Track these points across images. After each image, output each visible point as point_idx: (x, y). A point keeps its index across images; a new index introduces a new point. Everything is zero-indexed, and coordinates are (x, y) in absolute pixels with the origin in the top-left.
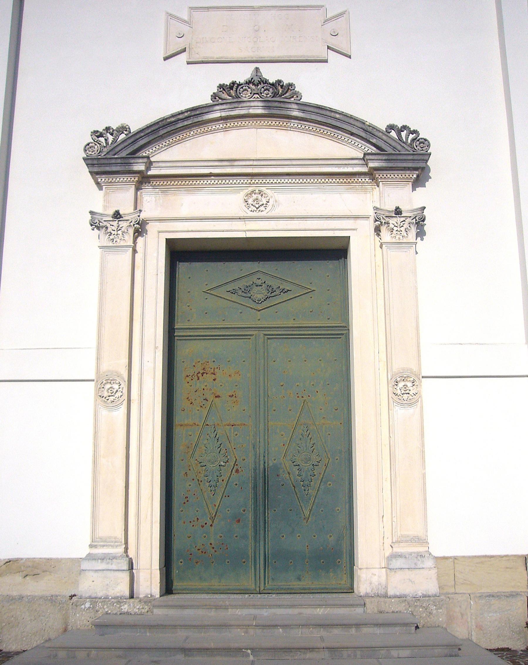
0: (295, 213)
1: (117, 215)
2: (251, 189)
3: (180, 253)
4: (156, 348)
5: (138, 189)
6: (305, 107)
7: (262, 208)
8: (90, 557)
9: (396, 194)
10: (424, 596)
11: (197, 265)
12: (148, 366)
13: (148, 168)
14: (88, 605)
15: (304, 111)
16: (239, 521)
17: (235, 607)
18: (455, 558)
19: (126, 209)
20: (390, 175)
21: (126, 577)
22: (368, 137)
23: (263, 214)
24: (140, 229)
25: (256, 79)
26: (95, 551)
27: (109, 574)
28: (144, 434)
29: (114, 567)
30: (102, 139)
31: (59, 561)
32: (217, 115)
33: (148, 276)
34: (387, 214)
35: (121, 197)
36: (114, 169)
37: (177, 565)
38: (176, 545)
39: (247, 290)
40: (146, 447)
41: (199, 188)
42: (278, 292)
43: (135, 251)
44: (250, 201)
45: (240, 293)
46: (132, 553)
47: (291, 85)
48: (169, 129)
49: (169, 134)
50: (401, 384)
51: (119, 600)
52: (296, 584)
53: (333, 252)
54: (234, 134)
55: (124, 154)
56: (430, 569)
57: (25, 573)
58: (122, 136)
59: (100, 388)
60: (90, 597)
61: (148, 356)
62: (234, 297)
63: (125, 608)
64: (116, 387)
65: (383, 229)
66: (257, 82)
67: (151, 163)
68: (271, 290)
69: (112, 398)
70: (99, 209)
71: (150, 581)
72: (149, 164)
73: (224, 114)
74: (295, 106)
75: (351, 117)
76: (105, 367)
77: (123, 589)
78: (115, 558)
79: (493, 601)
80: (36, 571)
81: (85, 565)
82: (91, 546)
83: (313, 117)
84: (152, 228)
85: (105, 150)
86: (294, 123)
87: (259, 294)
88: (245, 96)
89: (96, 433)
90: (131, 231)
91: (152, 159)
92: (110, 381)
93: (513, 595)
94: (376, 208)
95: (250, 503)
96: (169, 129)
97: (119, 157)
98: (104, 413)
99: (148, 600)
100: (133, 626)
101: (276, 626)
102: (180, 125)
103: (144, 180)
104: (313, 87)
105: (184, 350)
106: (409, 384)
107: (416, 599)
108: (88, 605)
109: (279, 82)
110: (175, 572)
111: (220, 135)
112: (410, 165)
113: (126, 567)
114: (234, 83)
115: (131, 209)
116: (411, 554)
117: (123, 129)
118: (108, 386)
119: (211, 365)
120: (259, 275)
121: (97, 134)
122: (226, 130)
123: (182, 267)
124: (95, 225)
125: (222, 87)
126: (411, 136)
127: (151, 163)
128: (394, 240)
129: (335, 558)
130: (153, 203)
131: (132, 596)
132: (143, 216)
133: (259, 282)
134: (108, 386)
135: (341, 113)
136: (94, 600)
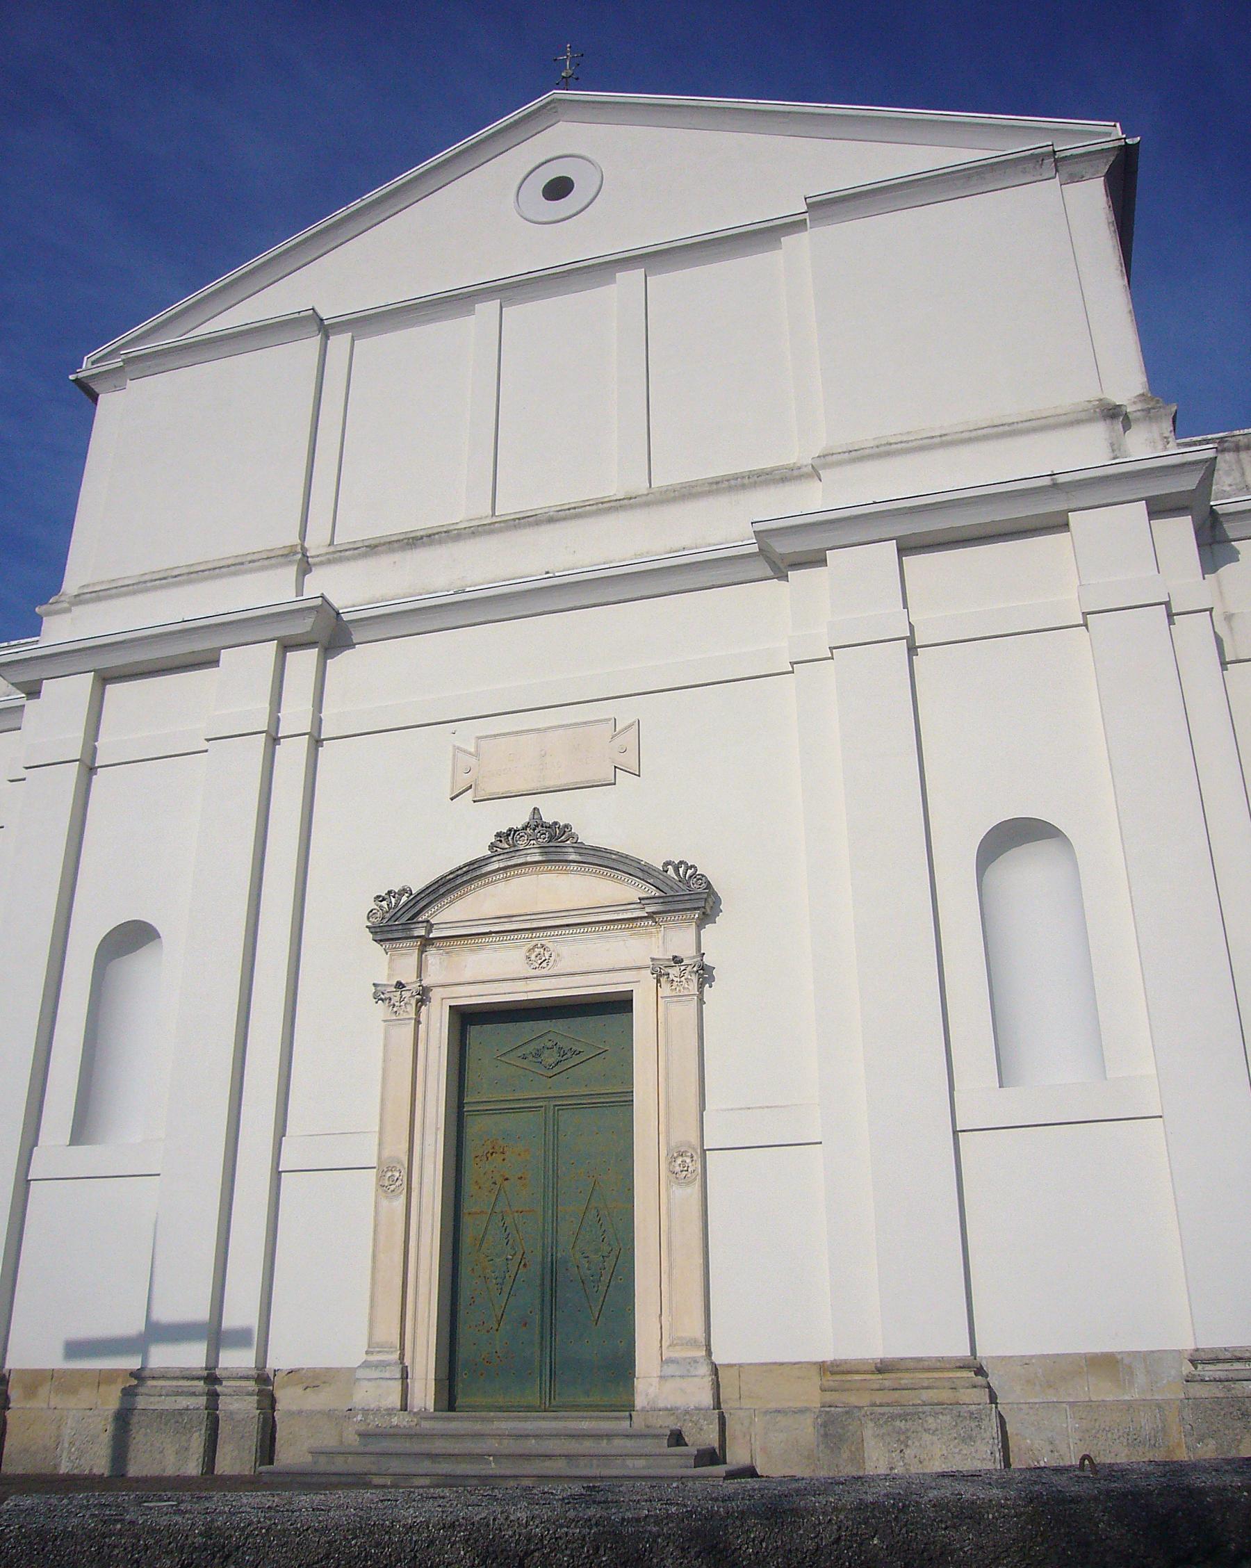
0: (580, 967)
1: (400, 985)
2: (533, 943)
3: (466, 1019)
4: (437, 1129)
5: (422, 951)
6: (581, 848)
7: (544, 964)
8: (366, 1365)
9: (677, 938)
10: (697, 1409)
11: (488, 1027)
12: (429, 1150)
13: (430, 931)
14: (359, 1417)
15: (580, 854)
16: (525, 1325)
17: (499, 1419)
18: (740, 1365)
19: (409, 977)
20: (669, 916)
21: (397, 1385)
22: (645, 877)
23: (544, 972)
24: (423, 997)
25: (533, 824)
26: (374, 1358)
27: (383, 1383)
28: (423, 1226)
29: (387, 1375)
30: (385, 904)
31: (338, 1370)
32: (496, 866)
33: (430, 1048)
34: (667, 963)
35: (405, 964)
36: (396, 935)
37: (462, 1375)
38: (463, 1353)
39: (538, 1054)
40: (426, 1240)
41: (481, 948)
42: (569, 1054)
43: (418, 1022)
44: (533, 957)
45: (531, 1058)
46: (407, 1362)
47: (566, 826)
48: (449, 886)
49: (449, 891)
50: (679, 1161)
51: (390, 1412)
52: (583, 1400)
53: (618, 1006)
54: (515, 882)
55: (403, 920)
56: (703, 1377)
57: (305, 1385)
58: (404, 899)
59: (380, 1178)
60: (363, 1409)
61: (430, 1139)
62: (525, 1064)
63: (395, 1421)
64: (397, 1174)
65: (663, 980)
66: (536, 825)
67: (432, 925)
68: (562, 1053)
69: (392, 1187)
70: (382, 980)
71: (424, 1393)
72: (430, 926)
73: (502, 865)
74: (571, 850)
75: (627, 857)
76: (386, 1153)
77: (395, 1400)
78: (389, 1365)
79: (780, 1417)
80: (317, 1383)
81: (360, 1374)
82: (367, 1353)
83: (590, 860)
84: (436, 995)
85: (388, 915)
86: (574, 866)
87: (550, 1058)
88: (522, 843)
89: (376, 1226)
90: (413, 1002)
91: (433, 921)
92: (390, 1169)
93: (802, 1411)
94: (653, 959)
95: (538, 1301)
96: (449, 886)
97: (402, 920)
98: (385, 1203)
99: (423, 1415)
100: (393, 1436)
101: (528, 1436)
102: (458, 882)
103: (426, 943)
104: (593, 820)
105: (474, 1127)
106: (688, 1160)
107: (687, 1412)
108: (359, 1417)
109: (556, 823)
110: (460, 1387)
111: (501, 885)
112: (688, 906)
113: (398, 1376)
114: (510, 830)
115: (414, 978)
116: (685, 1359)
117: (404, 891)
118: (389, 1174)
119: (501, 1142)
120: (549, 1036)
121: (379, 899)
122: (506, 879)
123: (474, 1031)
124: (377, 997)
125: (498, 835)
126: (689, 872)
127: (432, 925)
128: (674, 994)
129: (621, 1368)
130: (438, 967)
131: (404, 1408)
132: (424, 983)
133: (550, 1044)
134: (389, 1174)
135: (617, 854)
136: (365, 1411)
